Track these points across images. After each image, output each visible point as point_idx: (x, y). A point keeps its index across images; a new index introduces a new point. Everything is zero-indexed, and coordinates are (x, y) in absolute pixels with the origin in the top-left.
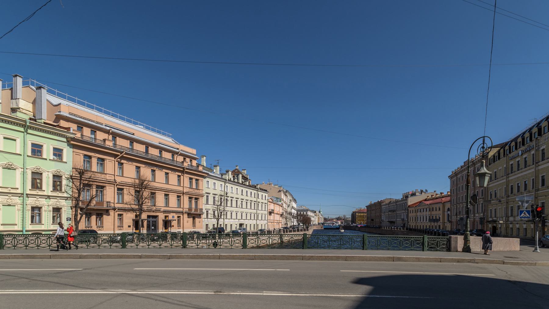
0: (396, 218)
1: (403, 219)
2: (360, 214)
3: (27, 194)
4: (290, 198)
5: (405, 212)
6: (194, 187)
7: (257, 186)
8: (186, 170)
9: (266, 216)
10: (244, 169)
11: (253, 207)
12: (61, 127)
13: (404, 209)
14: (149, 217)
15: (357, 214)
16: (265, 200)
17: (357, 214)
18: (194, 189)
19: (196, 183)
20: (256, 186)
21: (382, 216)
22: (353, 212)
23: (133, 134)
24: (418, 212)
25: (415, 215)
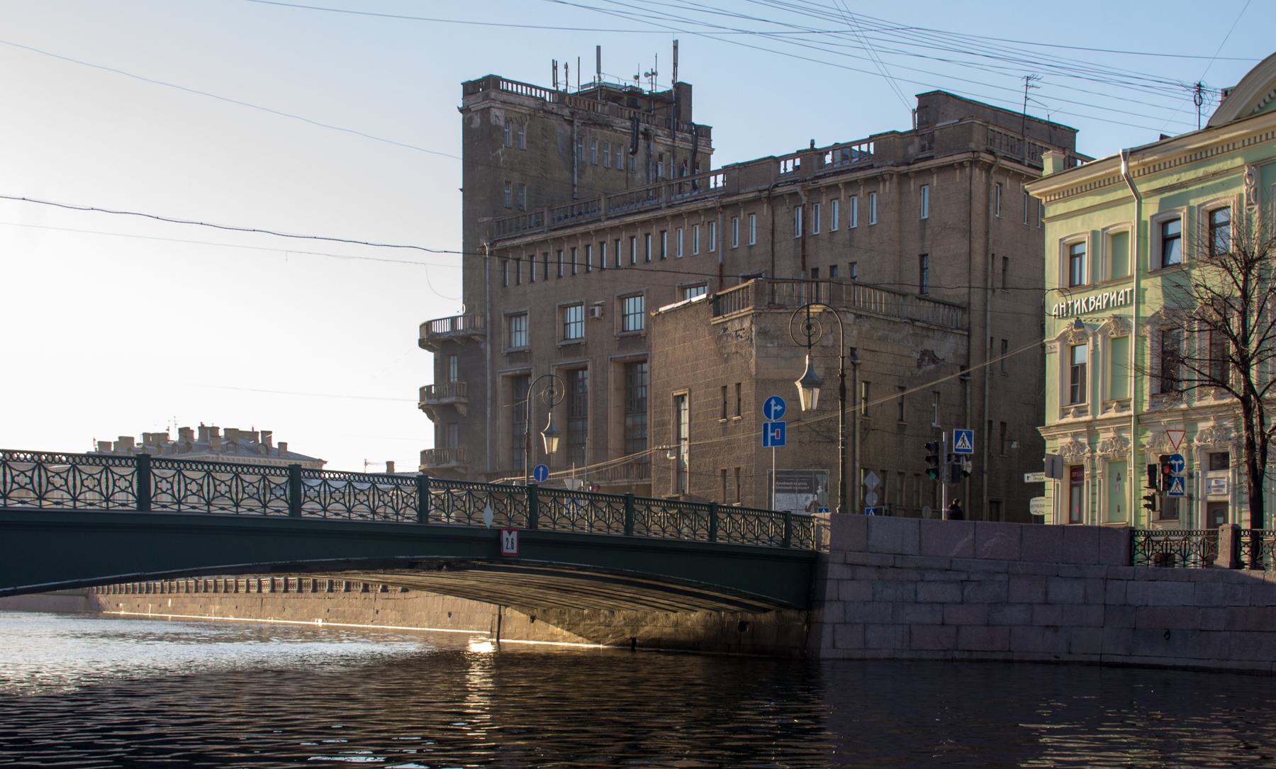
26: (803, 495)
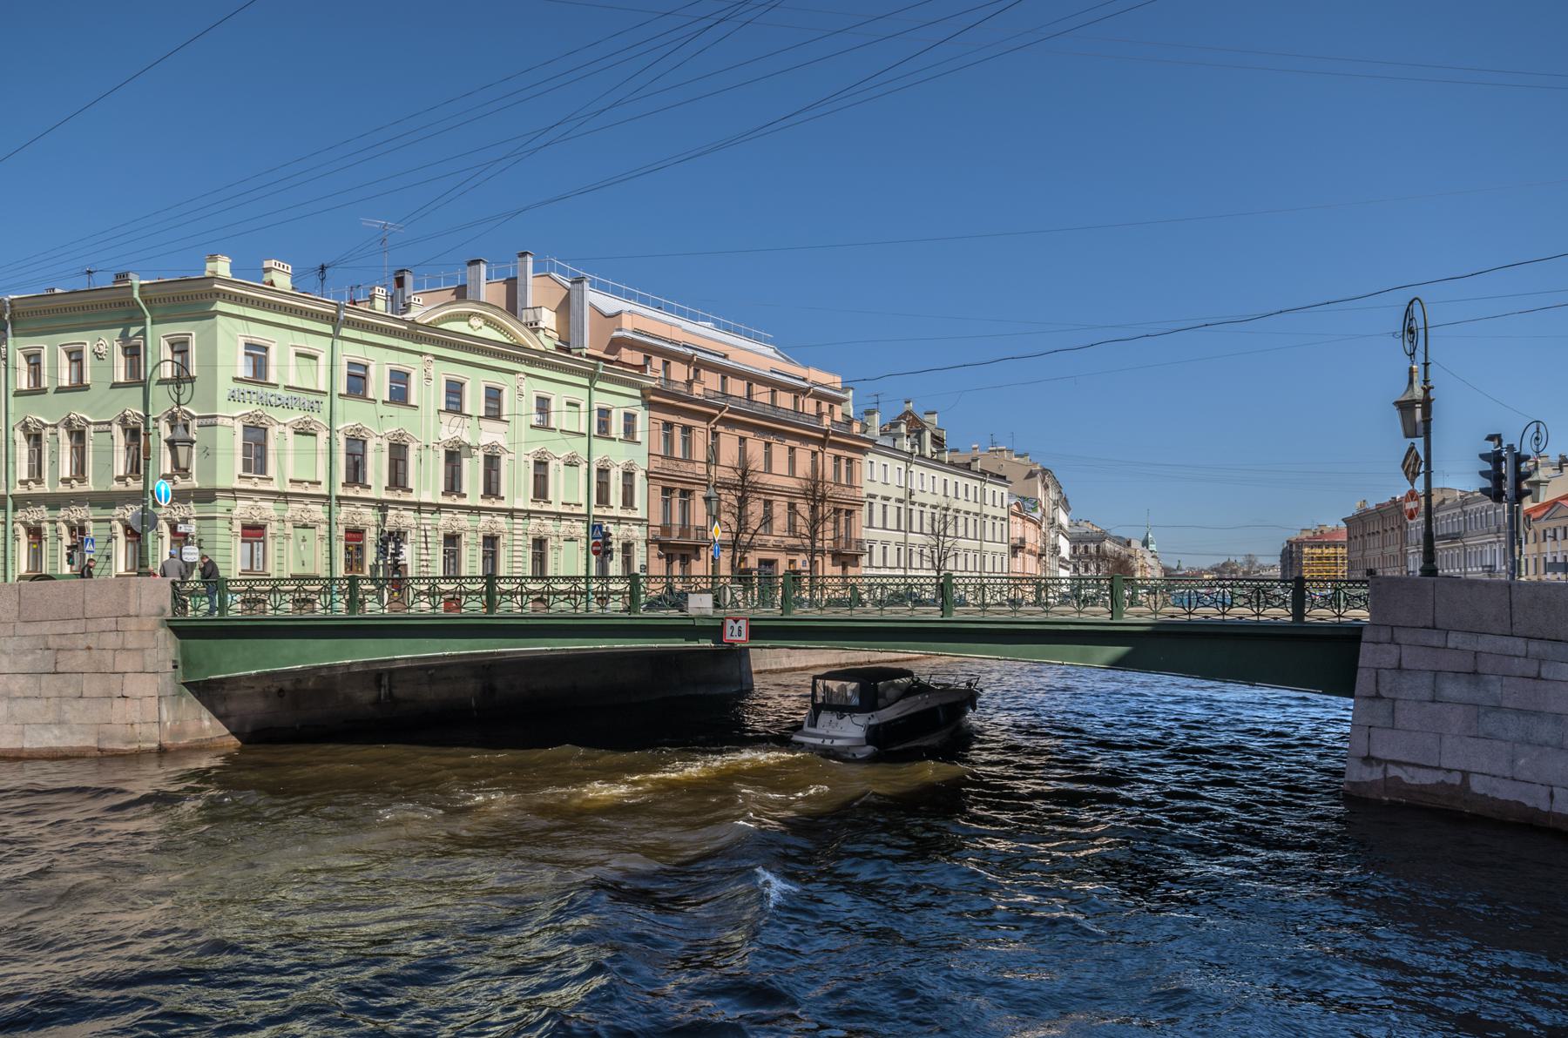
0: (1462, 565)
1: (1490, 566)
2: (1319, 551)
3: (339, 498)
4: (1053, 495)
5: (1499, 541)
6: (678, 453)
7: (973, 464)
8: (831, 438)
9: (1006, 558)
10: (932, 410)
11: (891, 523)
12: (624, 364)
13: (1494, 528)
14: (761, 562)
15: (1306, 550)
16: (1002, 507)
17: (1306, 550)
18: (677, 459)
19: (685, 439)
20: (969, 464)
21: (1411, 557)
22: (1290, 543)
23: (725, 357)
24: (1545, 540)
25: (1536, 551)
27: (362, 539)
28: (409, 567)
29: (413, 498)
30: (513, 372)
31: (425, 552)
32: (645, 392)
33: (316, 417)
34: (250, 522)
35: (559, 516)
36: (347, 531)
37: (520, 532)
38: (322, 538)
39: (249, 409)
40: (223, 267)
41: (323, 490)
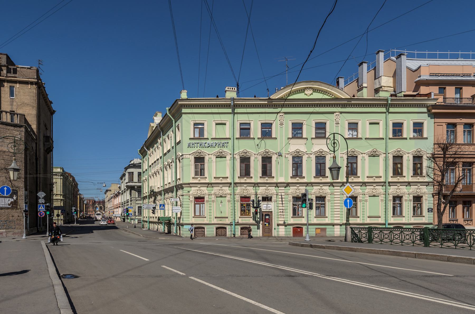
3: (389, 183)
26: (7, 198)
27: (324, 201)
28: (273, 212)
29: (274, 180)
30: (333, 113)
31: (281, 205)
32: (430, 108)
33: (225, 150)
34: (197, 196)
35: (209, 185)
36: (241, 197)
37: (339, 193)
38: (382, 200)
39: (195, 150)
40: (184, 95)
41: (382, 180)
